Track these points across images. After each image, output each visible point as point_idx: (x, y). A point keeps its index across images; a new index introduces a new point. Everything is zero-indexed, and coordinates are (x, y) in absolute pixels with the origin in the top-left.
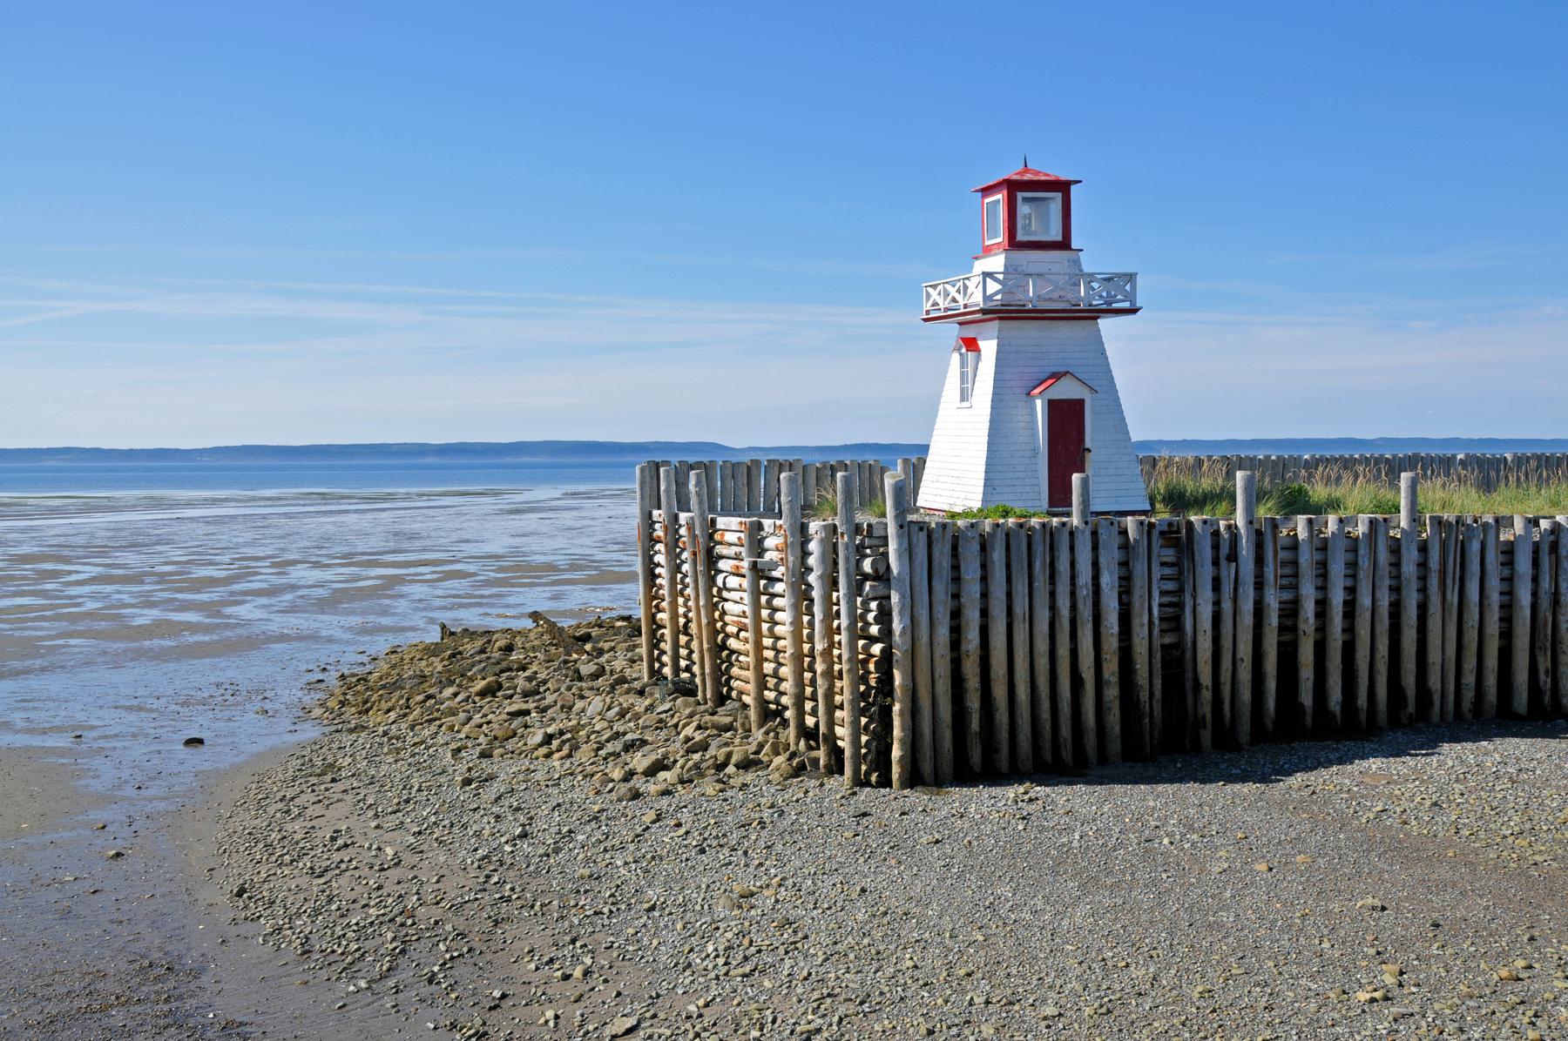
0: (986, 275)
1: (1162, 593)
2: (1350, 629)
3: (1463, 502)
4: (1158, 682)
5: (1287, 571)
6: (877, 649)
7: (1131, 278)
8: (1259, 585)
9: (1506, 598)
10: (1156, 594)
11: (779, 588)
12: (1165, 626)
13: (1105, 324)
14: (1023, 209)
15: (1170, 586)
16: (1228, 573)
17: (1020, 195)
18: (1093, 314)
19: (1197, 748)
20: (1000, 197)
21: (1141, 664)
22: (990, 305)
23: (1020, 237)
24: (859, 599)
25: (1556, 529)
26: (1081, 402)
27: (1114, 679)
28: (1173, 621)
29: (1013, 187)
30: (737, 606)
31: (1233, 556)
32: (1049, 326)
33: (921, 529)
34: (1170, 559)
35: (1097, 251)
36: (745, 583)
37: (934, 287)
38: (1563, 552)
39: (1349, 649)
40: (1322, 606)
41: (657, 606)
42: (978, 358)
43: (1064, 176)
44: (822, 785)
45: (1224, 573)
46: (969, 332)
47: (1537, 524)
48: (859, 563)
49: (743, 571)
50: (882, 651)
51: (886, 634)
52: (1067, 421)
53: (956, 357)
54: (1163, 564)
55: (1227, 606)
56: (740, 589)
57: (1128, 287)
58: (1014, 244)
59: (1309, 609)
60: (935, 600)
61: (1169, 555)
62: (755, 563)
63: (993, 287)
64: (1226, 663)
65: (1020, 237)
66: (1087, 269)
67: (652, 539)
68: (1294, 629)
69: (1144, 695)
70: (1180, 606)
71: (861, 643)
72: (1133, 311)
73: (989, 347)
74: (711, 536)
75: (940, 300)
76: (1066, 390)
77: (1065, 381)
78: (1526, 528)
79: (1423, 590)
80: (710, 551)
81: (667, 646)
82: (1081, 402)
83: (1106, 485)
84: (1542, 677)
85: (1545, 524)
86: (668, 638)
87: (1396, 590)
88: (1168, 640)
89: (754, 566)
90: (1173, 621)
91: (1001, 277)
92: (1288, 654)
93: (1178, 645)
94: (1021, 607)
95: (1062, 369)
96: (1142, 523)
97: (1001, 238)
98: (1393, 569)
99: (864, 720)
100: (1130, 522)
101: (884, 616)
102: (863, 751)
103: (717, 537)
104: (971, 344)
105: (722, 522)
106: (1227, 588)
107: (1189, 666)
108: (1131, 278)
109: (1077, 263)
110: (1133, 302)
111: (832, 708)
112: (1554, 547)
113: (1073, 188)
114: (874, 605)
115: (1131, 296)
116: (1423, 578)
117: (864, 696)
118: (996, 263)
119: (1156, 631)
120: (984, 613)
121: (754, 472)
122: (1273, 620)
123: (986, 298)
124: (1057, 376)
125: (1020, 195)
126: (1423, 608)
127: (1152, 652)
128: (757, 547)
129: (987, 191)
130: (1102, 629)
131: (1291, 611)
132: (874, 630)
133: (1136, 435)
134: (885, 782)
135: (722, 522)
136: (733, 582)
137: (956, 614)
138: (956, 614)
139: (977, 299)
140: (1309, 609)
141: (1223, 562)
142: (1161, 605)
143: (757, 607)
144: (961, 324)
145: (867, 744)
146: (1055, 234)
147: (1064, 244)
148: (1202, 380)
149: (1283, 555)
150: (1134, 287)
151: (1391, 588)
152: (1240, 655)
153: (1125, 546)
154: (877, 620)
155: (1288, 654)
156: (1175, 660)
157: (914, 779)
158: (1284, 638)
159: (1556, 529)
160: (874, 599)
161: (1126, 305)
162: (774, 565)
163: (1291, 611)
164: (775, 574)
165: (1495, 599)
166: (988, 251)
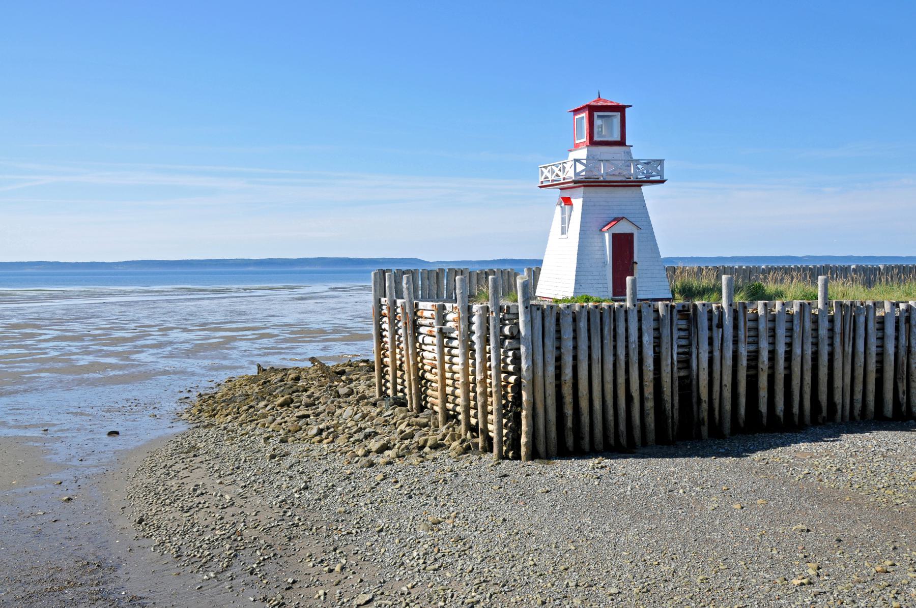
0: (576, 160)
1: (679, 346)
2: (789, 367)
3: (855, 293)
4: (676, 398)
5: (752, 333)
6: (512, 379)
7: (661, 162)
8: (736, 342)
9: (879, 349)
10: (675, 347)
11: (455, 343)
13: (645, 189)
14: (598, 122)
15: (684, 342)
16: (717, 335)
17: (596, 114)
19: (699, 437)
20: (584, 115)
22: (579, 178)
23: (596, 138)
25: (909, 309)
26: (632, 235)
27: (651, 397)
28: (685, 363)
29: (592, 109)
30: (431, 354)
31: (720, 325)
32: (612, 190)
33: (538, 309)
34: (683, 327)
35: (641, 147)
36: (435, 340)
37: (546, 167)
38: (913, 322)
39: (788, 379)
40: (772, 354)
41: (384, 354)
42: (572, 209)
43: (622, 103)
46: (566, 194)
47: (898, 306)
48: (501, 329)
49: (434, 334)
51: (518, 370)
52: (623, 246)
53: (558, 208)
54: (679, 329)
55: (717, 354)
56: (432, 344)
57: (659, 168)
58: (592, 142)
59: (764, 356)
60: (546, 350)
61: (683, 324)
62: (441, 329)
63: (580, 168)
64: (716, 388)
65: (596, 138)
66: (635, 157)
67: (381, 315)
68: (756, 367)
69: (668, 406)
70: (689, 354)
71: (503, 375)
73: (578, 203)
74: (415, 313)
75: (549, 175)
76: (623, 228)
78: (892, 309)
79: (831, 345)
80: (415, 322)
81: (389, 377)
82: (632, 235)
84: (901, 395)
85: (902, 306)
86: (390, 372)
87: (816, 344)
88: (682, 374)
89: (441, 330)
90: (685, 363)
91: (585, 162)
92: (752, 382)
93: (689, 377)
94: (596, 354)
95: (621, 216)
96: (667, 305)
97: (585, 139)
100: (660, 305)
101: (517, 360)
102: (504, 439)
103: (419, 313)
105: (422, 305)
106: (717, 344)
108: (661, 162)
109: (629, 153)
110: (662, 176)
111: (486, 413)
112: (908, 320)
113: (627, 110)
114: (510, 353)
115: (661, 173)
116: (831, 338)
117: (505, 406)
118: (582, 153)
119: (675, 369)
120: (575, 358)
121: (440, 275)
123: (576, 174)
124: (617, 220)
125: (596, 114)
126: (831, 355)
128: (443, 320)
129: (577, 111)
130: (644, 368)
131: (754, 357)
133: (664, 254)
134: (517, 457)
135: (422, 305)
136: (428, 340)
137: (558, 359)
138: (558, 359)
139: (570, 175)
140: (764, 356)
141: (715, 328)
142: (678, 353)
143: (442, 355)
144: (561, 189)
145: (507, 435)
146: (617, 137)
147: (622, 143)
148: (703, 222)
149: (749, 324)
150: (662, 168)
151: (813, 344)
152: (724, 382)
153: (657, 319)
154: (512, 362)
155: (752, 382)
156: (686, 386)
157: (534, 455)
158: (750, 373)
159: (909, 309)
160: (511, 350)
161: (658, 178)
162: (452, 330)
163: (754, 357)
164: (453, 335)
165: (873, 350)
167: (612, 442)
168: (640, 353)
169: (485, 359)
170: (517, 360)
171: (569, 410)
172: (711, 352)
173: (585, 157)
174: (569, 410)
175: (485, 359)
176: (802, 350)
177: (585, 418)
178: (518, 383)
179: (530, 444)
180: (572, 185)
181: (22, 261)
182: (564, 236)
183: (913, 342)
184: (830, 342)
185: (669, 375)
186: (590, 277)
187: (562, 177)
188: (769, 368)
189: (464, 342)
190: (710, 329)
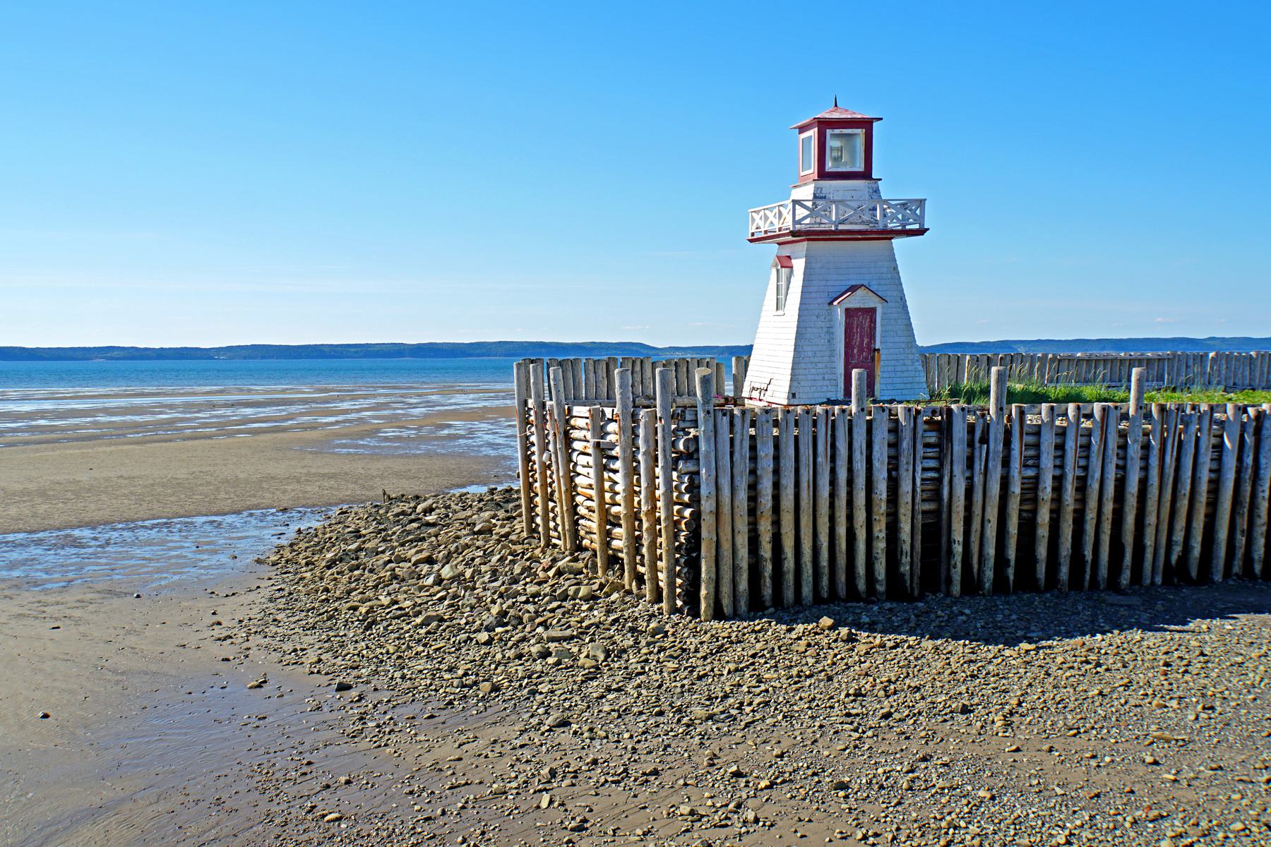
0: (795, 202)
1: (924, 470)
2: (1082, 500)
5: (1031, 453)
6: (687, 513)
7: (921, 203)
8: (1006, 463)
9: (1213, 475)
10: (919, 469)
11: (618, 465)
12: (925, 496)
13: (896, 242)
14: (831, 143)
15: (932, 464)
17: (829, 132)
18: (888, 234)
20: (813, 133)
21: (905, 527)
24: (675, 474)
25: (1260, 416)
26: (872, 311)
27: (883, 535)
29: (824, 125)
31: (985, 440)
32: (850, 251)
33: (724, 415)
34: (933, 440)
35: (894, 184)
36: (591, 460)
37: (771, 209)
38: (1265, 433)
40: (1059, 481)
42: (791, 272)
43: (869, 115)
44: (851, 639)
45: (977, 454)
46: (786, 250)
47: (1245, 411)
48: (674, 444)
49: (590, 451)
50: (691, 514)
52: (860, 324)
53: (774, 271)
54: (927, 445)
55: (978, 479)
56: (588, 466)
58: (823, 175)
59: (1047, 483)
60: (736, 471)
61: (932, 438)
63: (801, 212)
64: (976, 525)
65: (830, 166)
67: (528, 423)
70: (939, 480)
71: (676, 508)
72: (921, 232)
73: (799, 265)
74: (567, 421)
75: (761, 224)
76: (859, 300)
77: (860, 292)
78: (1235, 415)
79: (1145, 468)
80: (566, 433)
81: (539, 510)
82: (872, 311)
83: (905, 391)
84: (1239, 536)
85: (1251, 411)
86: (540, 504)
89: (597, 445)
91: (809, 204)
93: (937, 513)
95: (858, 283)
96: (909, 410)
97: (813, 170)
98: (1120, 452)
99: (678, 568)
101: (694, 488)
102: (678, 590)
103: (573, 422)
104: (785, 262)
105: (577, 410)
106: (979, 466)
107: (944, 532)
108: (921, 203)
109: (877, 191)
110: (922, 224)
111: (655, 558)
112: (1258, 432)
113: (875, 124)
115: (920, 219)
116: (1145, 458)
117: (678, 549)
121: (612, 366)
122: (1016, 489)
123: (795, 222)
124: (853, 289)
125: (829, 132)
126: (1144, 483)
127: (970, 526)
128: (601, 432)
129: (802, 129)
130: (874, 496)
131: (1032, 487)
132: (686, 498)
134: (695, 613)
135: (577, 410)
136: (582, 460)
138: (753, 487)
139: (788, 224)
140: (1047, 483)
141: (977, 445)
142: (923, 480)
143: (600, 480)
146: (859, 167)
147: (866, 174)
148: (953, 299)
149: (1030, 439)
150: (923, 212)
151: (1117, 466)
152: (988, 516)
153: (895, 429)
154: (688, 490)
157: (718, 614)
158: (1025, 507)
159: (1260, 416)
161: (916, 226)
162: (612, 446)
163: (1032, 487)
164: (613, 453)
165: (1205, 476)
166: (803, 182)
167: (861, 585)
168: (776, 499)
169: (652, 487)
170: (694, 488)
171: (766, 551)
172: (970, 479)
173: (811, 197)
174: (766, 551)
175: (652, 487)
176: (1102, 475)
177: (789, 564)
178: (696, 516)
179: (712, 597)
180: (790, 238)
181: (87, 346)
182: (780, 312)
183: (1263, 461)
184: (1143, 464)
185: (910, 507)
186: (813, 371)
187: (777, 226)
188: (1052, 500)
189: (626, 466)
190: (971, 444)
